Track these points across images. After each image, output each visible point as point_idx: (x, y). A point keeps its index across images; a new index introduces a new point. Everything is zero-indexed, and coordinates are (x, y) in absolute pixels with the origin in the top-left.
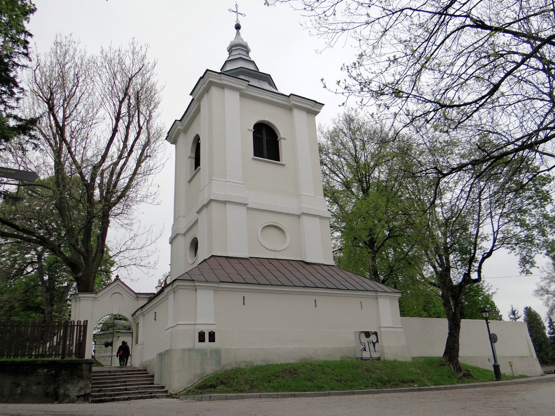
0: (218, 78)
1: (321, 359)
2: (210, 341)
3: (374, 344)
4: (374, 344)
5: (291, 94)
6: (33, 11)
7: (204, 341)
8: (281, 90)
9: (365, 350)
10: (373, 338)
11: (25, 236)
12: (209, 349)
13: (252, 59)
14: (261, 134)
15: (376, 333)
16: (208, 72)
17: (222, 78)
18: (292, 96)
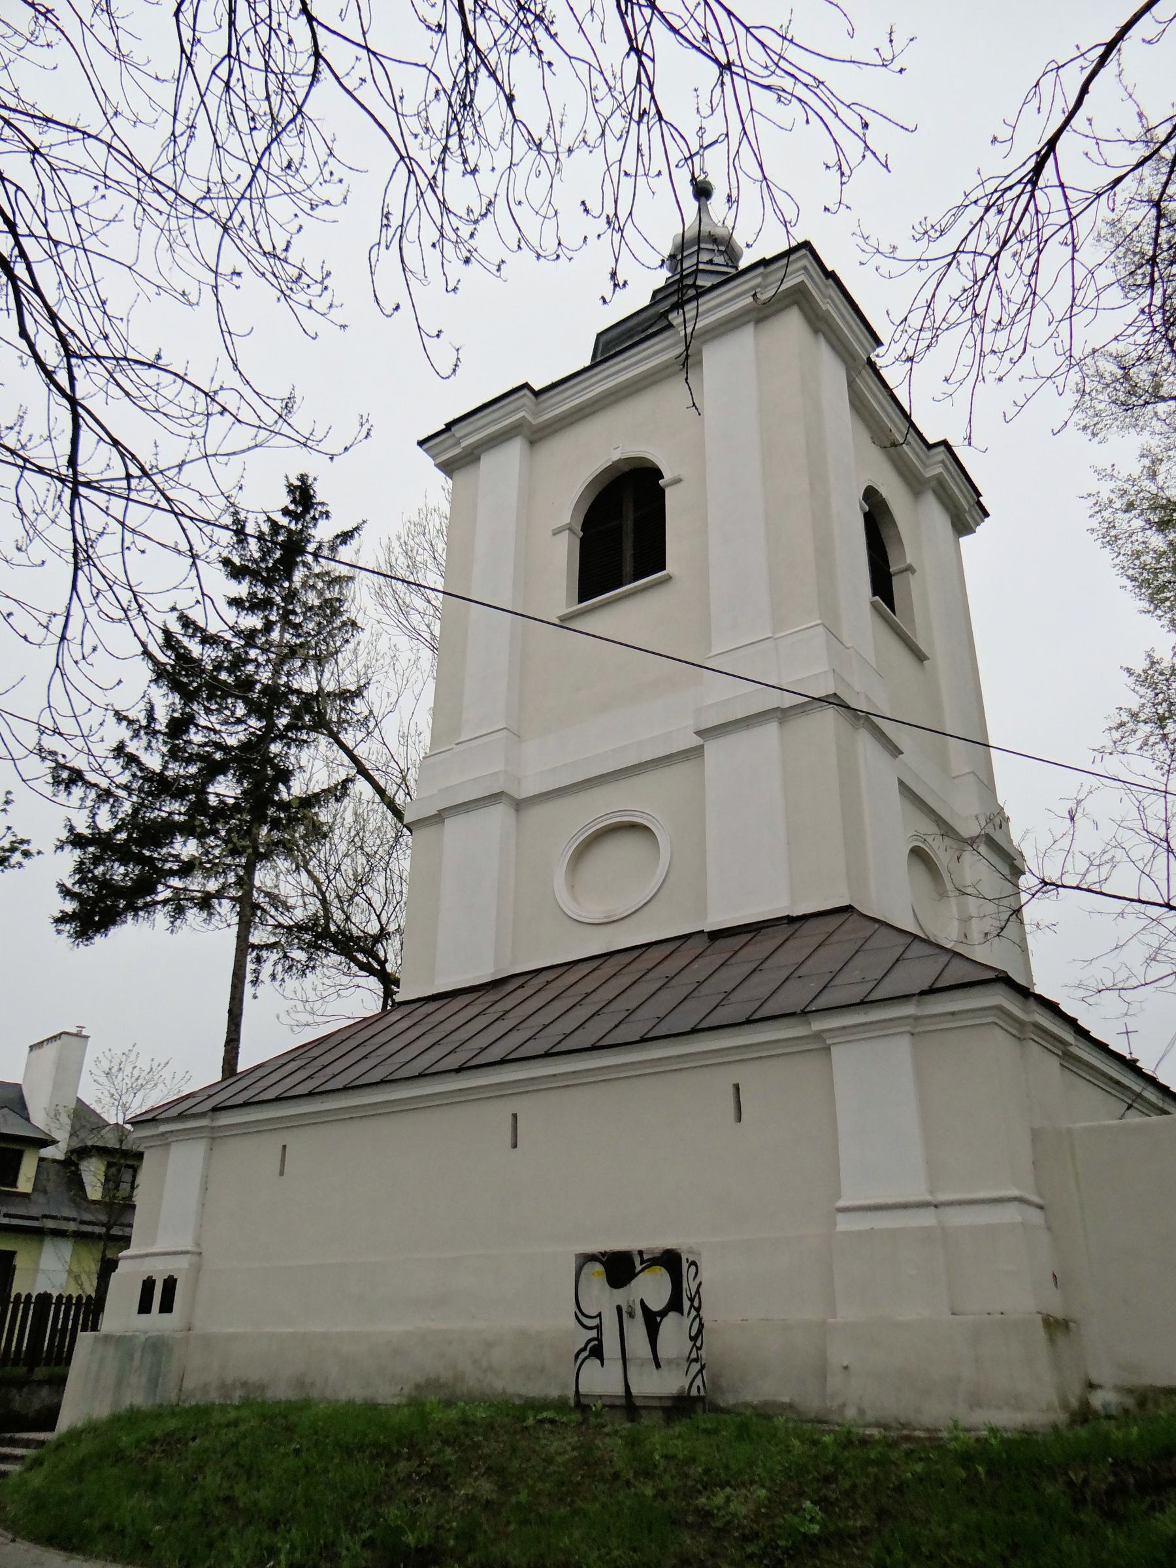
0: (451, 442)
1: (499, 1385)
3: (652, 1322)
4: (652, 1322)
9: (596, 1351)
10: (652, 1288)
12: (143, 1338)
15: (670, 1261)
17: (458, 435)
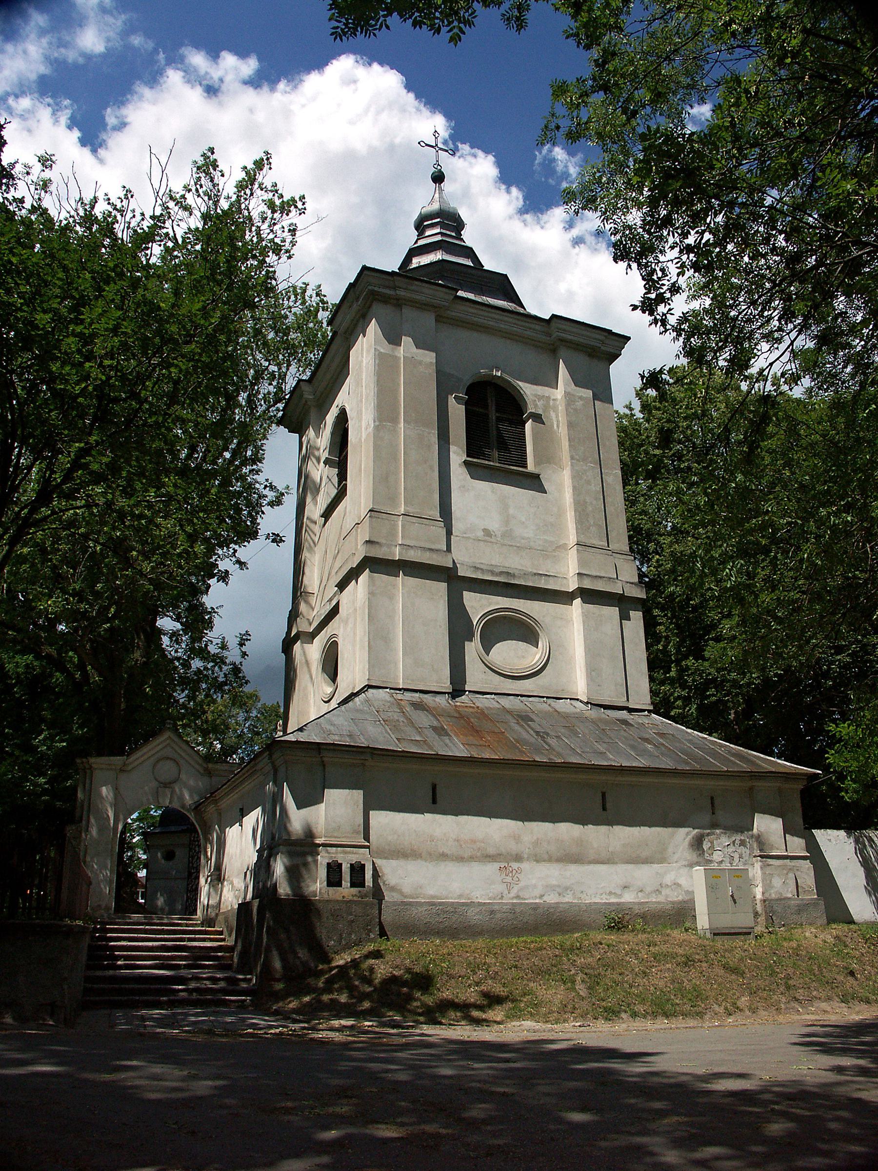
2: (353, 885)
5: (554, 316)
6: (54, 124)
7: (339, 884)
8: (532, 308)
11: (11, 469)
13: (468, 243)
14: (486, 407)
16: (366, 272)
17: (397, 284)
18: (555, 320)
